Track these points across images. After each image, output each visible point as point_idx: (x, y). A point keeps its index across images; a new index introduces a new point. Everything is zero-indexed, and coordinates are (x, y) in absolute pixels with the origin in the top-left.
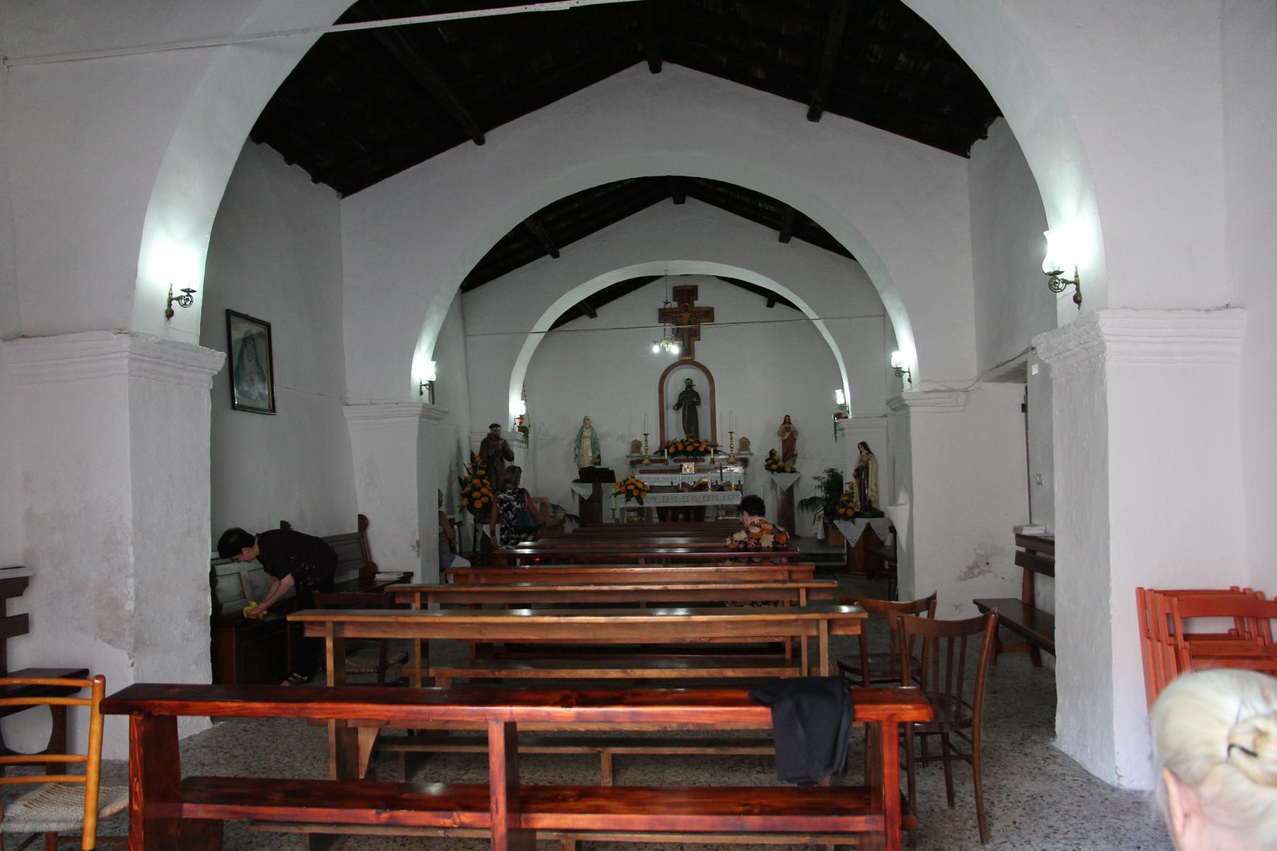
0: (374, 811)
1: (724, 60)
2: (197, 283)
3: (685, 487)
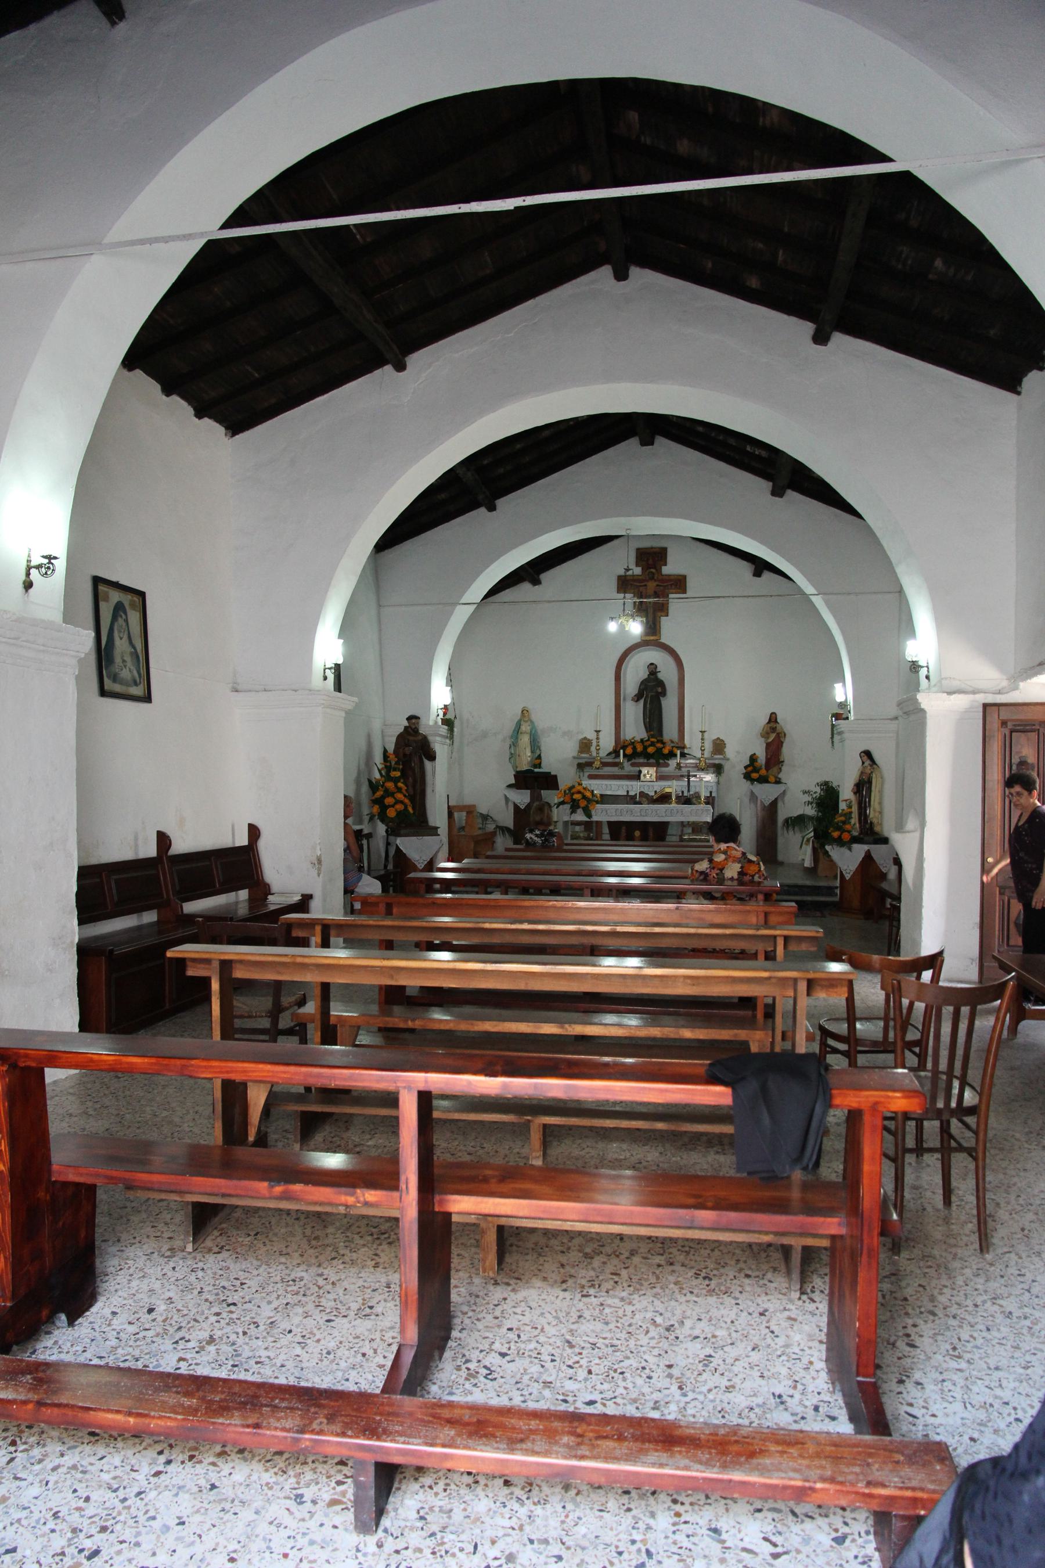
0: (266, 1184)
1: (710, 265)
2: (60, 548)
3: (644, 798)
